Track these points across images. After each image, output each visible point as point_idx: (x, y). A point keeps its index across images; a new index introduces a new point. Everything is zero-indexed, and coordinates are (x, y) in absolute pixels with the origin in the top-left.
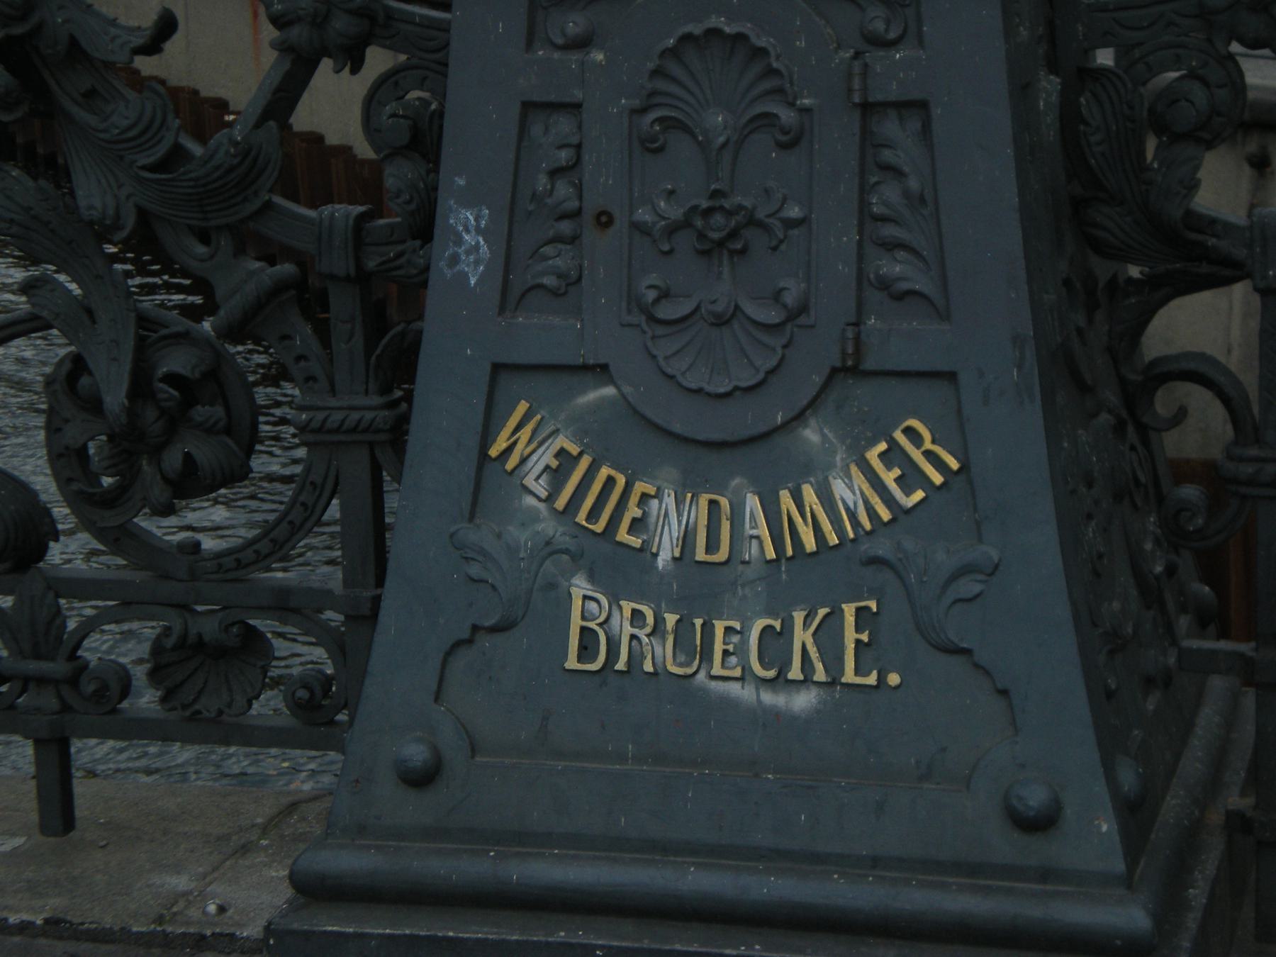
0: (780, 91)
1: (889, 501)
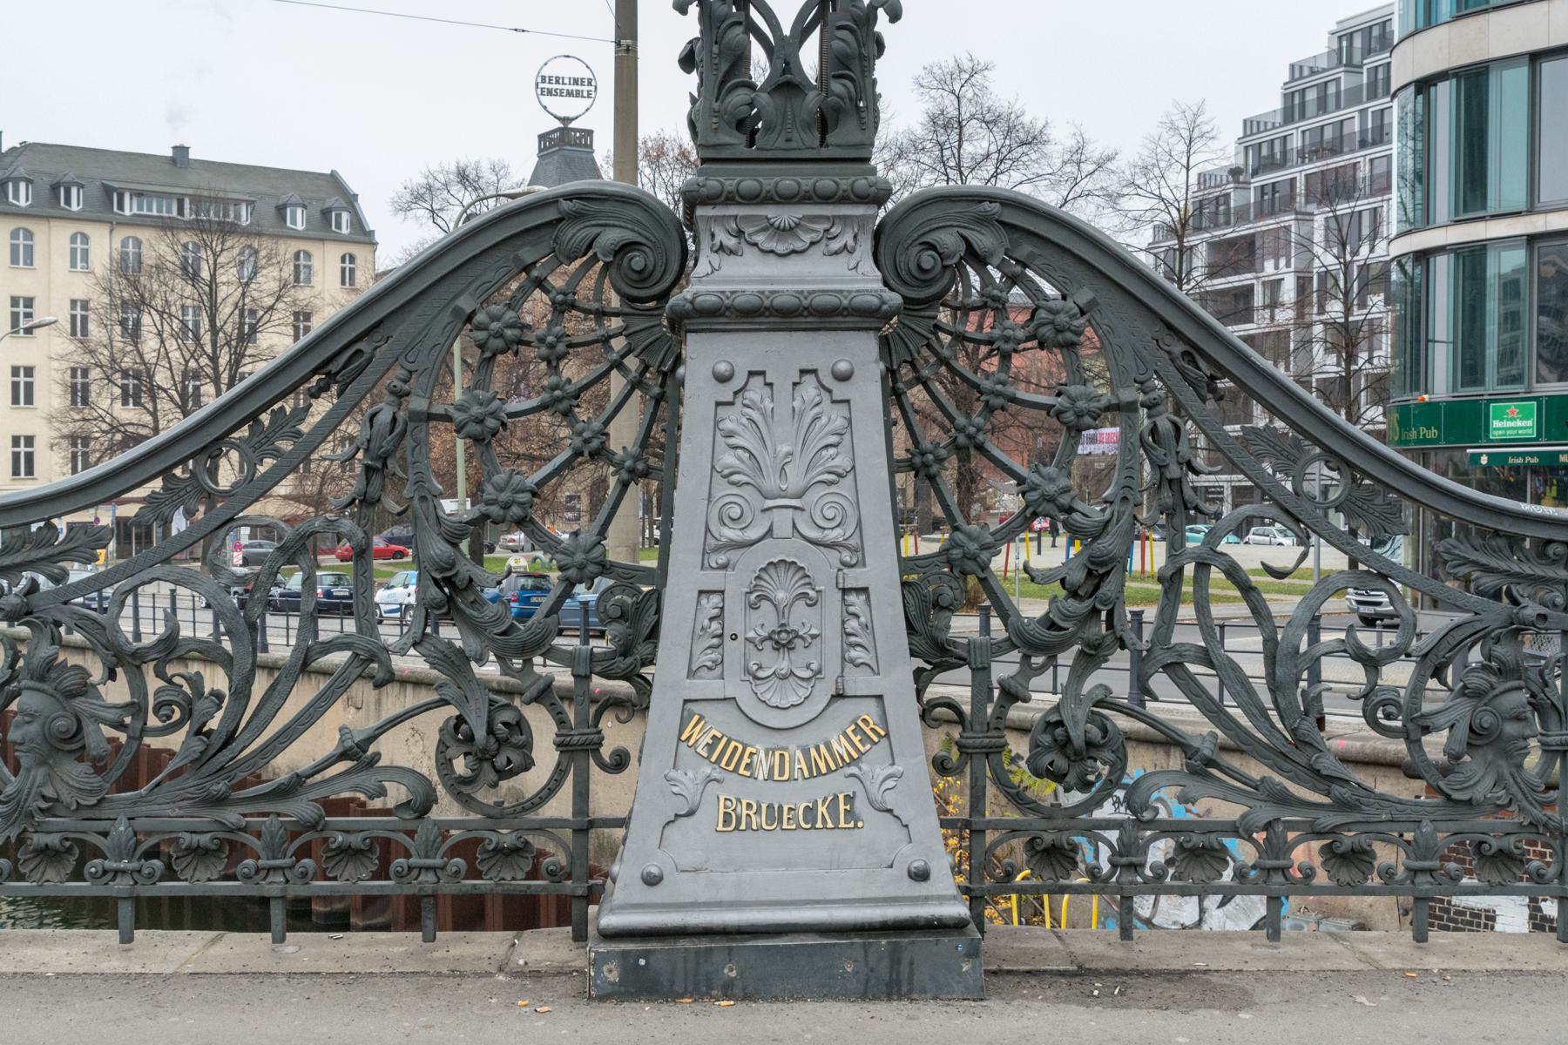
0: (810, 584)
1: (857, 750)
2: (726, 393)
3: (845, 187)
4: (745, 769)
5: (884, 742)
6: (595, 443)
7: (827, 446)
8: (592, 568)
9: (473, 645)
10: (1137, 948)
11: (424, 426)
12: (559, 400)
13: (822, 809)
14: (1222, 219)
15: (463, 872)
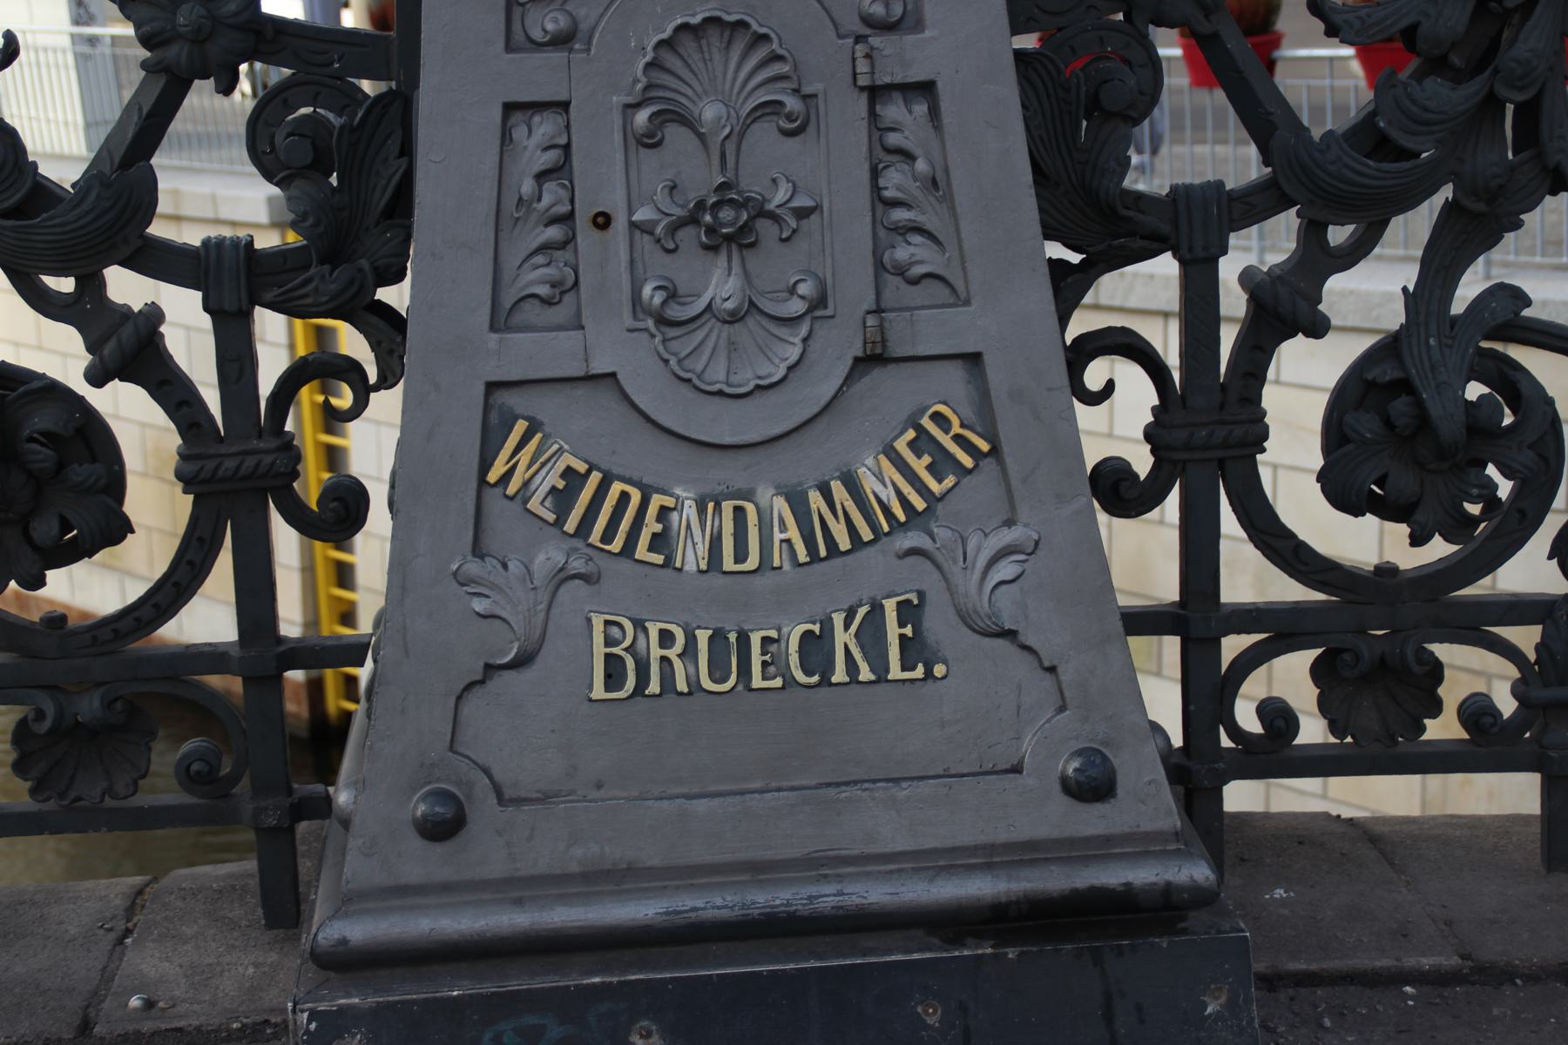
1: (923, 490)
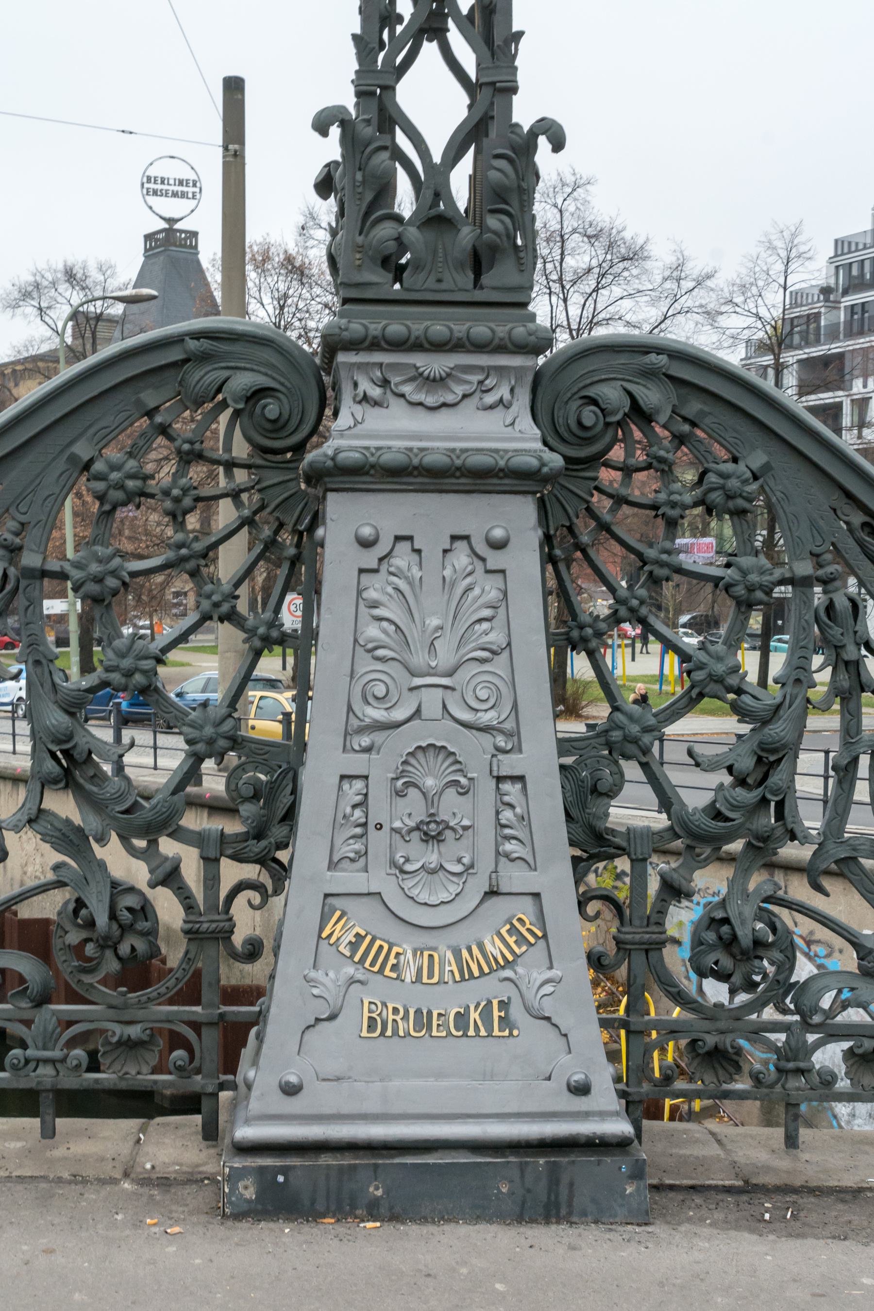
1: (512, 952)
2: (369, 559)
3: (501, 335)
4: (391, 970)
5: (542, 943)
6: (225, 608)
7: (480, 621)
8: (222, 743)
9: (92, 823)
10: (806, 1156)
11: (38, 582)
12: (184, 559)
13: (474, 1015)
14: (812, 337)
15: (84, 1065)
